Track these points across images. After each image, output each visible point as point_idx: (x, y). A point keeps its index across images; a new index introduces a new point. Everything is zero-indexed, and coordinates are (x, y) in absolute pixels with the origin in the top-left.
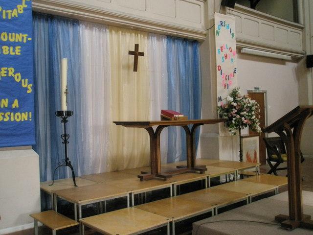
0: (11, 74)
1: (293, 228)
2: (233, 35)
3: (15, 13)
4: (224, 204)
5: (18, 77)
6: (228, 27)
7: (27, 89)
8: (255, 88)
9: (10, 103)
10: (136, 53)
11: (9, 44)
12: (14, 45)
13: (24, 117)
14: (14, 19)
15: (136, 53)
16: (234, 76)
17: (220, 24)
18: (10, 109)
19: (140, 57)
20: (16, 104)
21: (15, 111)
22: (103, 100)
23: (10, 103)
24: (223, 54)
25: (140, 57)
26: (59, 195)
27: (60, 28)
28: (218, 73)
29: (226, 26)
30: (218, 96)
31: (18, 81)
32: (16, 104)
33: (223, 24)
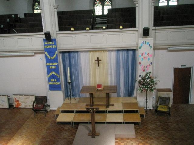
0: (54, 73)
1: (142, 117)
2: (151, 47)
3: (53, 58)
4: (20, 94)
5: (56, 74)
6: (148, 43)
7: (58, 77)
8: (181, 66)
9: (54, 80)
10: (98, 60)
11: (53, 66)
12: (54, 66)
13: (58, 83)
14: (53, 59)
15: (98, 60)
16: (150, 66)
17: (142, 43)
18: (54, 81)
19: (99, 62)
20: (56, 80)
21: (56, 82)
22: (112, 68)
23: (54, 80)
24: (143, 57)
25: (99, 62)
26: (10, 93)
27: (72, 54)
28: (139, 65)
29: (147, 44)
30: (140, 73)
31: (56, 75)
32: (56, 80)
33: (144, 43)
